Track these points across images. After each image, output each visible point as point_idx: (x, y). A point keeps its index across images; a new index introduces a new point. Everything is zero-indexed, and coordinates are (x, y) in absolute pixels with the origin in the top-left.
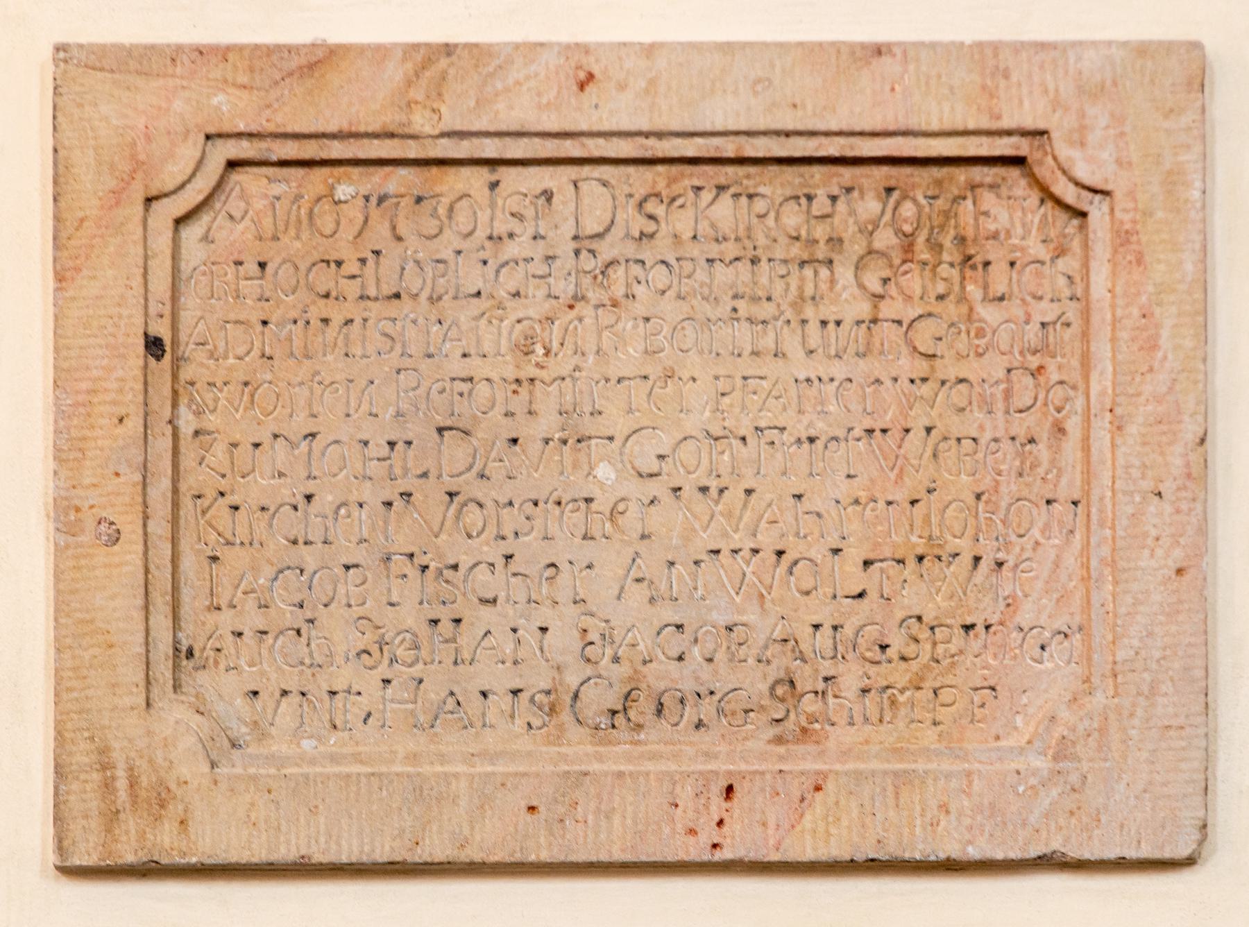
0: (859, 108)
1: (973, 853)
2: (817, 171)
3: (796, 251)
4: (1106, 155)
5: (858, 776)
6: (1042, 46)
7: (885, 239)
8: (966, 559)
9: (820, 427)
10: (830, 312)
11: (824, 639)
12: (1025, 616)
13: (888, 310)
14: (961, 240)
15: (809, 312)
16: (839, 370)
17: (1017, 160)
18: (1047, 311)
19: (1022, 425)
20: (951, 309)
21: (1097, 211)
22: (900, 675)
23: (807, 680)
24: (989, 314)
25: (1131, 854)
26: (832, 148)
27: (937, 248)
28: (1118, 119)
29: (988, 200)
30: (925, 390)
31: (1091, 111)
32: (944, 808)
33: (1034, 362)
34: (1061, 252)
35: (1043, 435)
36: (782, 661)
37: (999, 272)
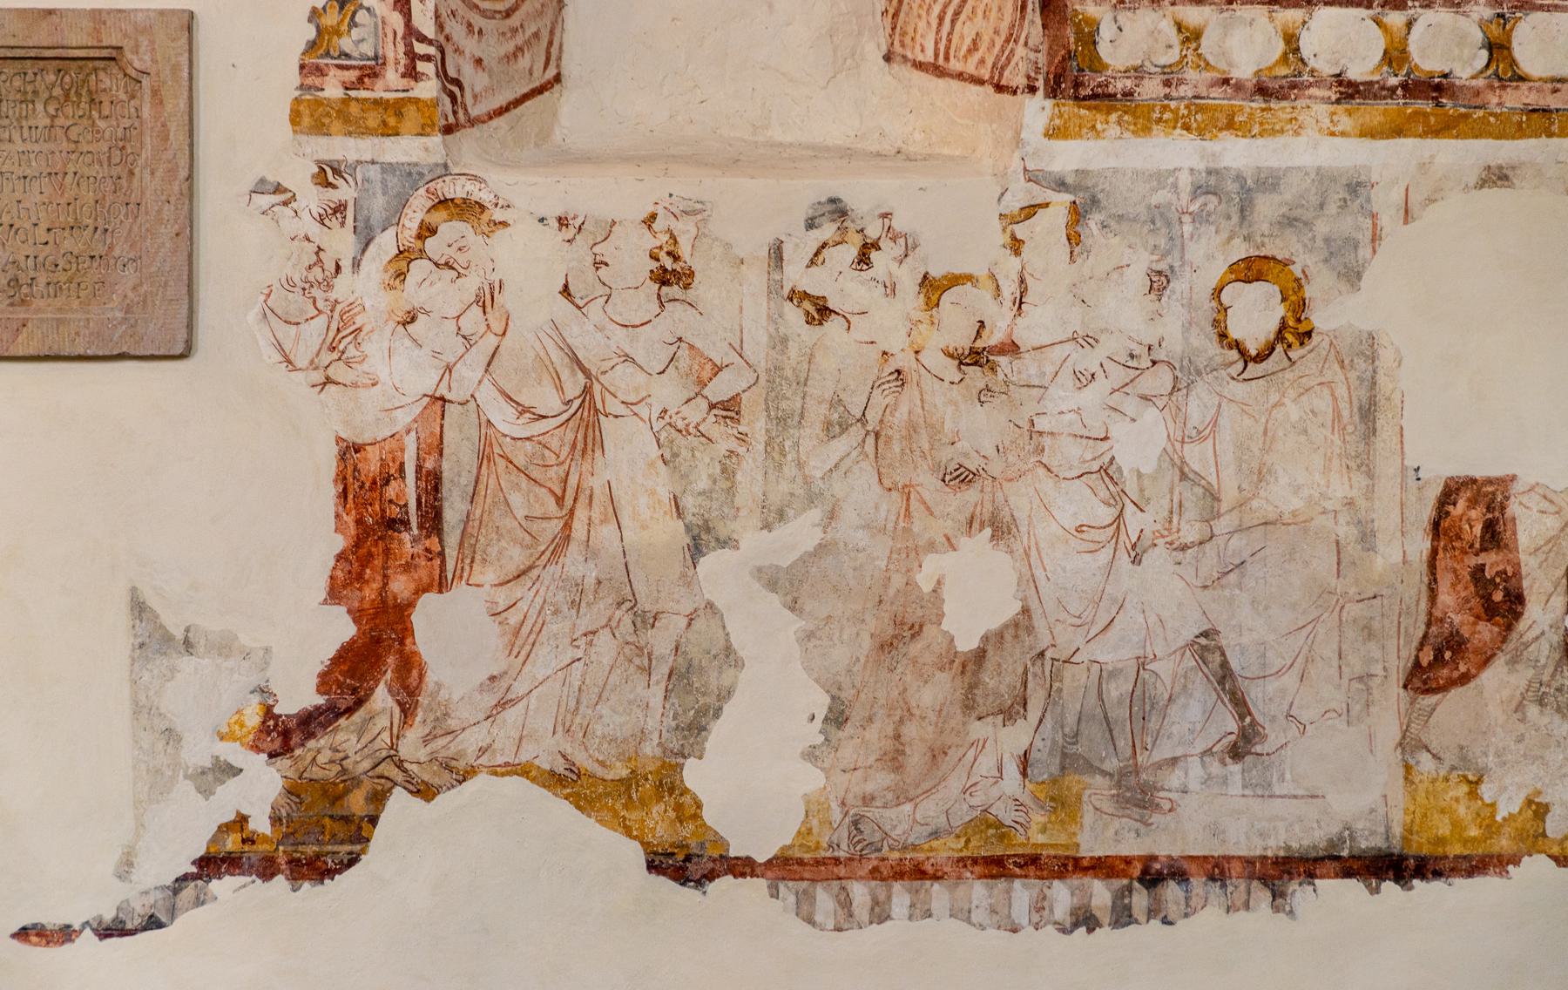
0: (42, 36)
1: (89, 352)
2: (29, 62)
3: (18, 96)
4: (147, 58)
5: (42, 320)
6: (120, 11)
7: (57, 92)
8: (91, 228)
9: (28, 172)
10: (32, 122)
11: (30, 262)
12: (117, 253)
13: (60, 121)
14: (90, 92)
15: (24, 123)
16: (36, 148)
17: (113, 57)
18: (126, 123)
19: (115, 171)
20: (85, 121)
21: (145, 81)
22: (63, 277)
23: (23, 279)
24: (101, 124)
25: (156, 353)
26: (32, 53)
27: (79, 95)
28: (152, 42)
29: (102, 75)
30: (73, 157)
31: (141, 39)
32: (77, 334)
33: (121, 144)
34: (133, 97)
35: (124, 175)
36: (12, 272)
37: (106, 105)
